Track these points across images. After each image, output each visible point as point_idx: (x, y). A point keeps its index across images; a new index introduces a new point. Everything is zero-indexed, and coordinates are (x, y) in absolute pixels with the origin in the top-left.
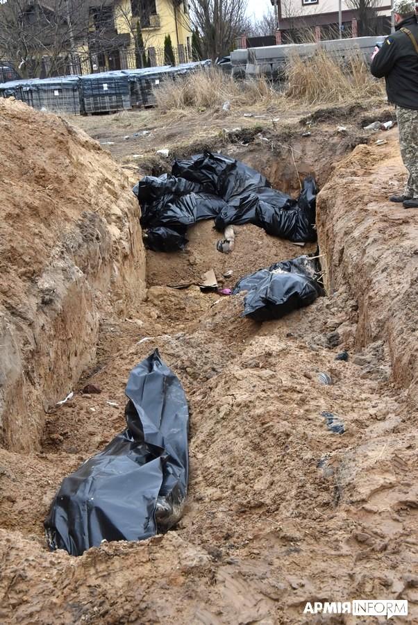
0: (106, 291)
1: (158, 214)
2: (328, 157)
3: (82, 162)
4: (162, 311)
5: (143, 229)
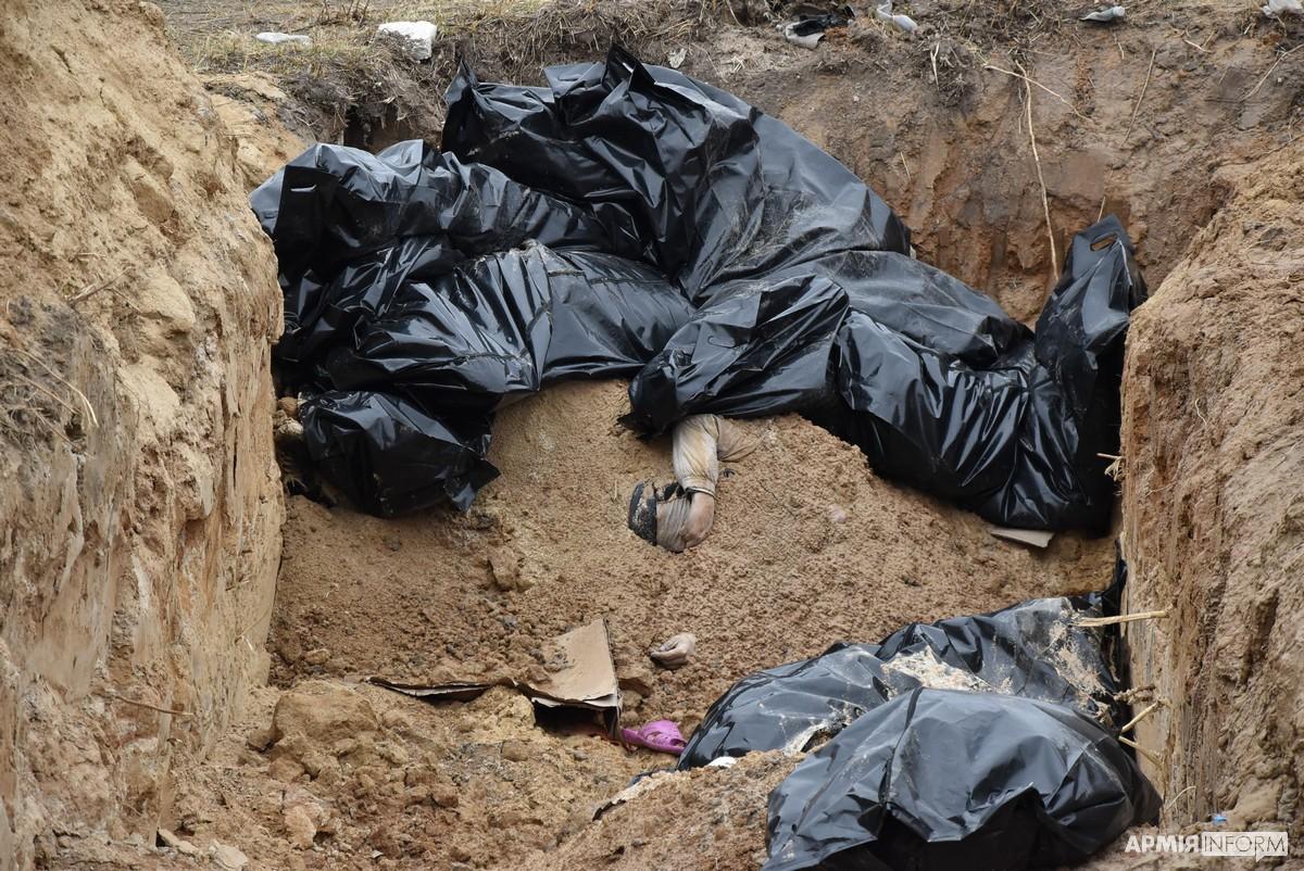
0: (83, 689)
1: (362, 330)
2: (1201, 136)
3: (21, 48)
4: (340, 807)
5: (280, 394)
